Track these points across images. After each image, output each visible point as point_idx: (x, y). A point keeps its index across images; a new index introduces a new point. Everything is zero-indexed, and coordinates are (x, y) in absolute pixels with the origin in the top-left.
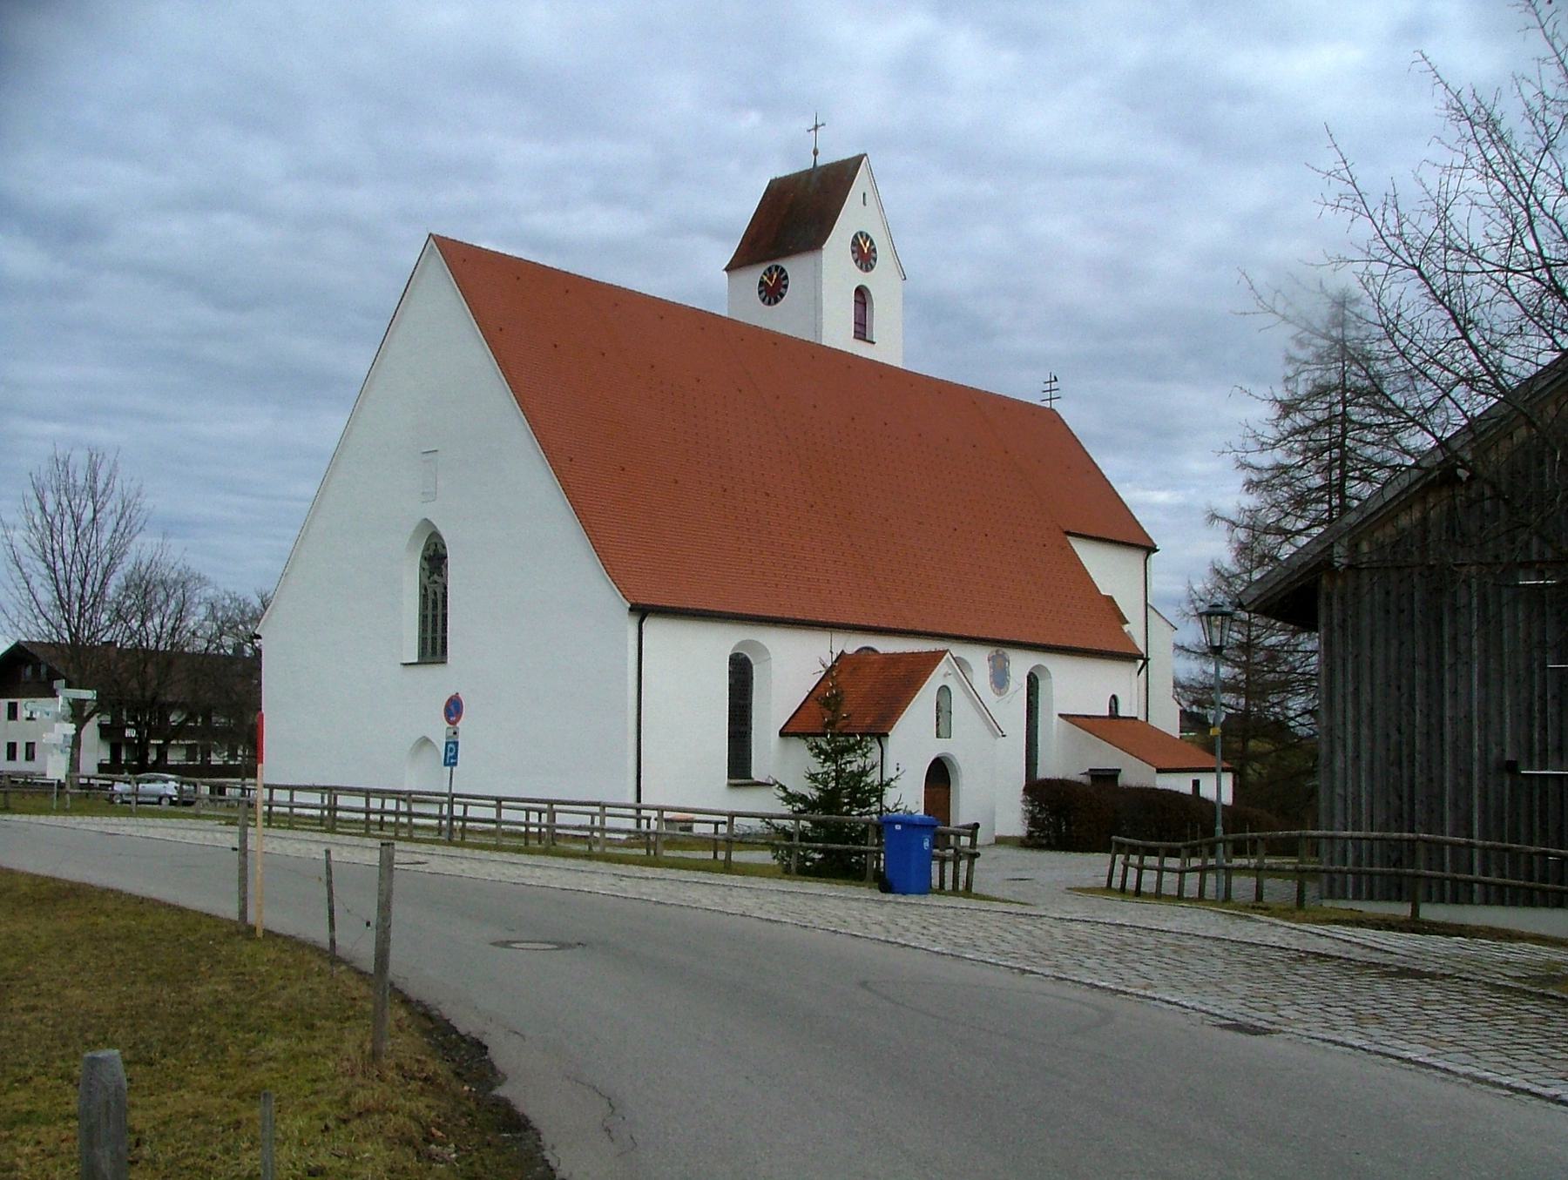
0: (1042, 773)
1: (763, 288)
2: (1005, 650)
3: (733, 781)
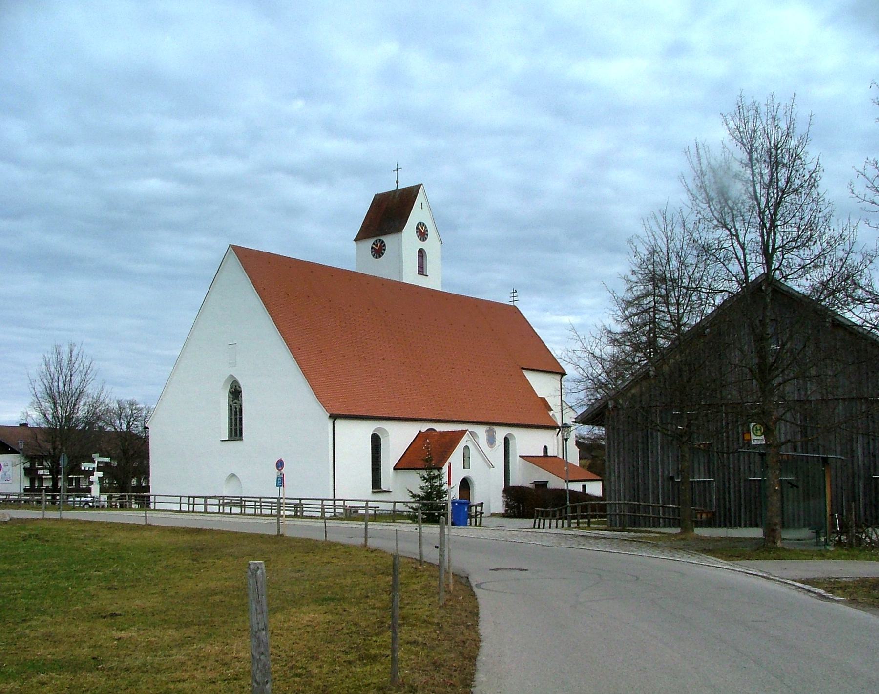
0: (512, 484)
1: (373, 250)
2: (493, 427)
3: (375, 490)
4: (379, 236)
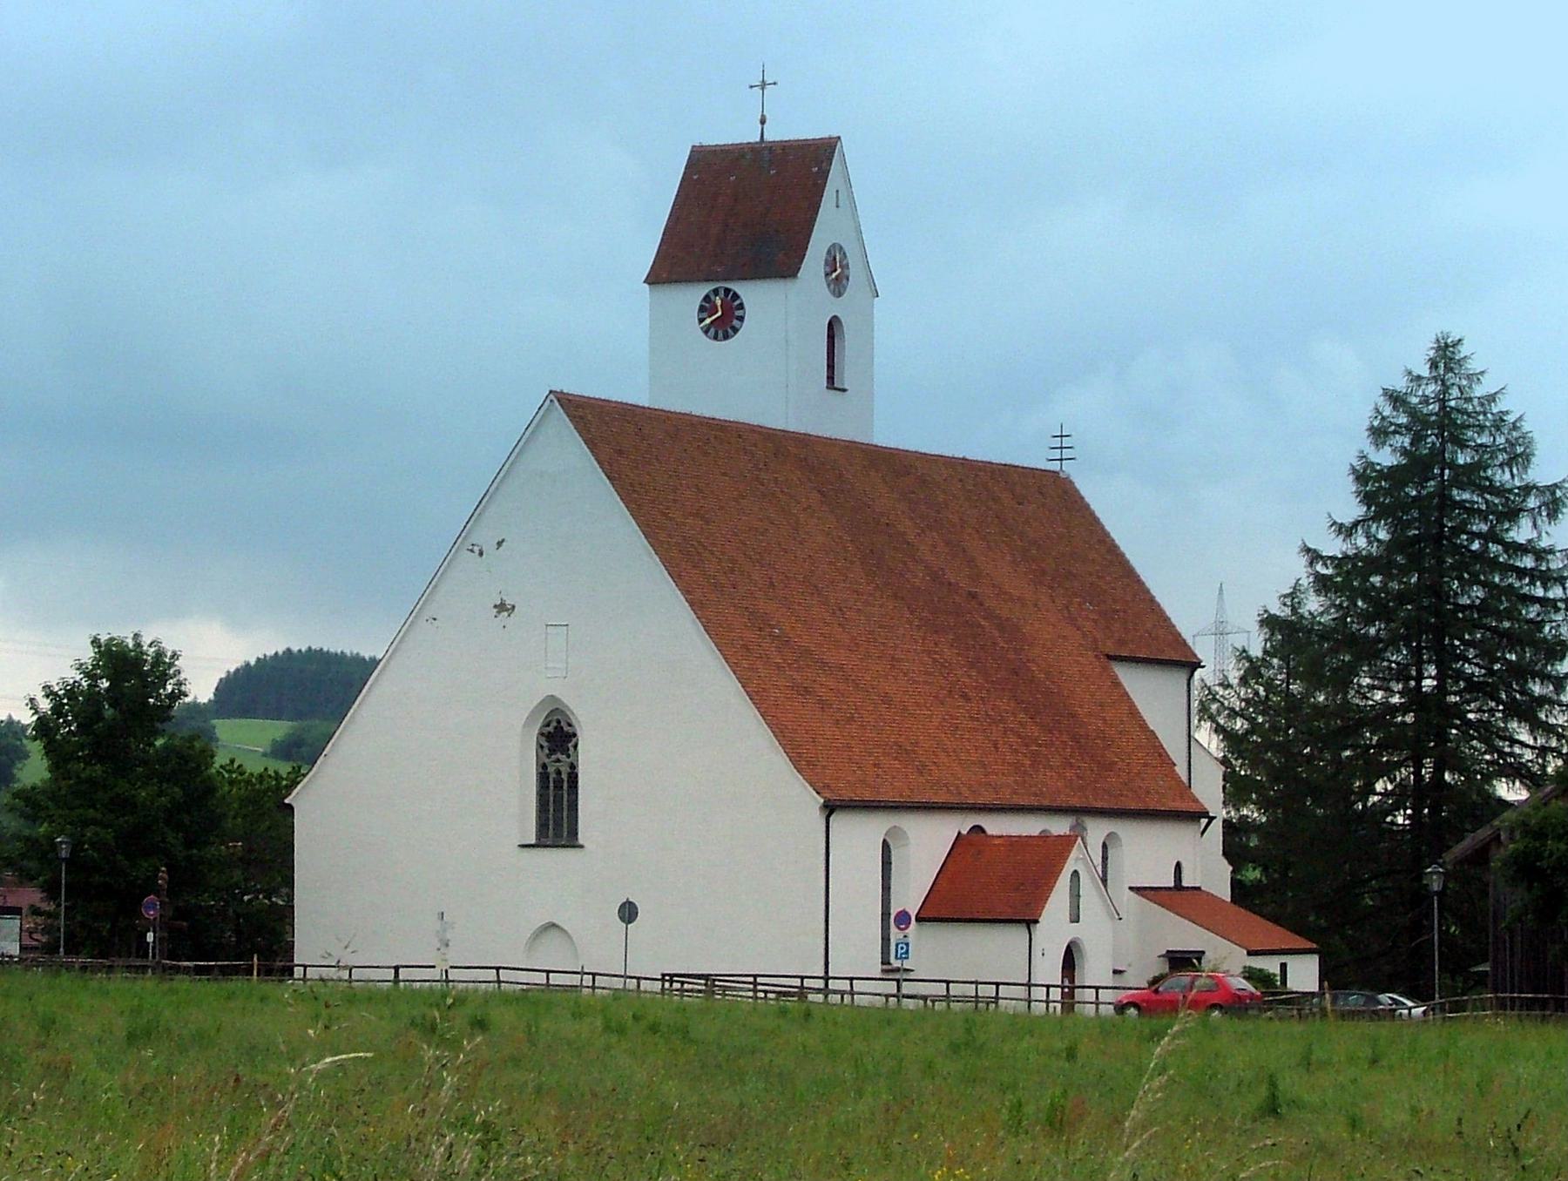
4: (726, 280)
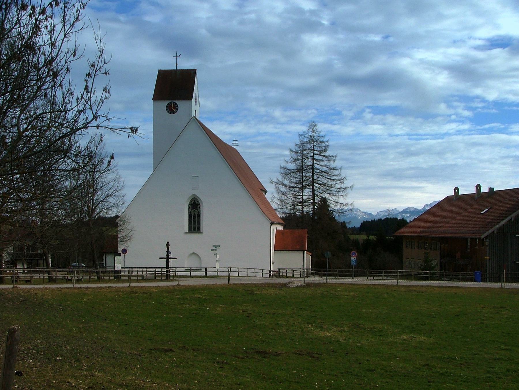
4: (174, 100)
